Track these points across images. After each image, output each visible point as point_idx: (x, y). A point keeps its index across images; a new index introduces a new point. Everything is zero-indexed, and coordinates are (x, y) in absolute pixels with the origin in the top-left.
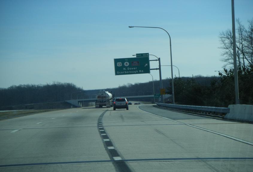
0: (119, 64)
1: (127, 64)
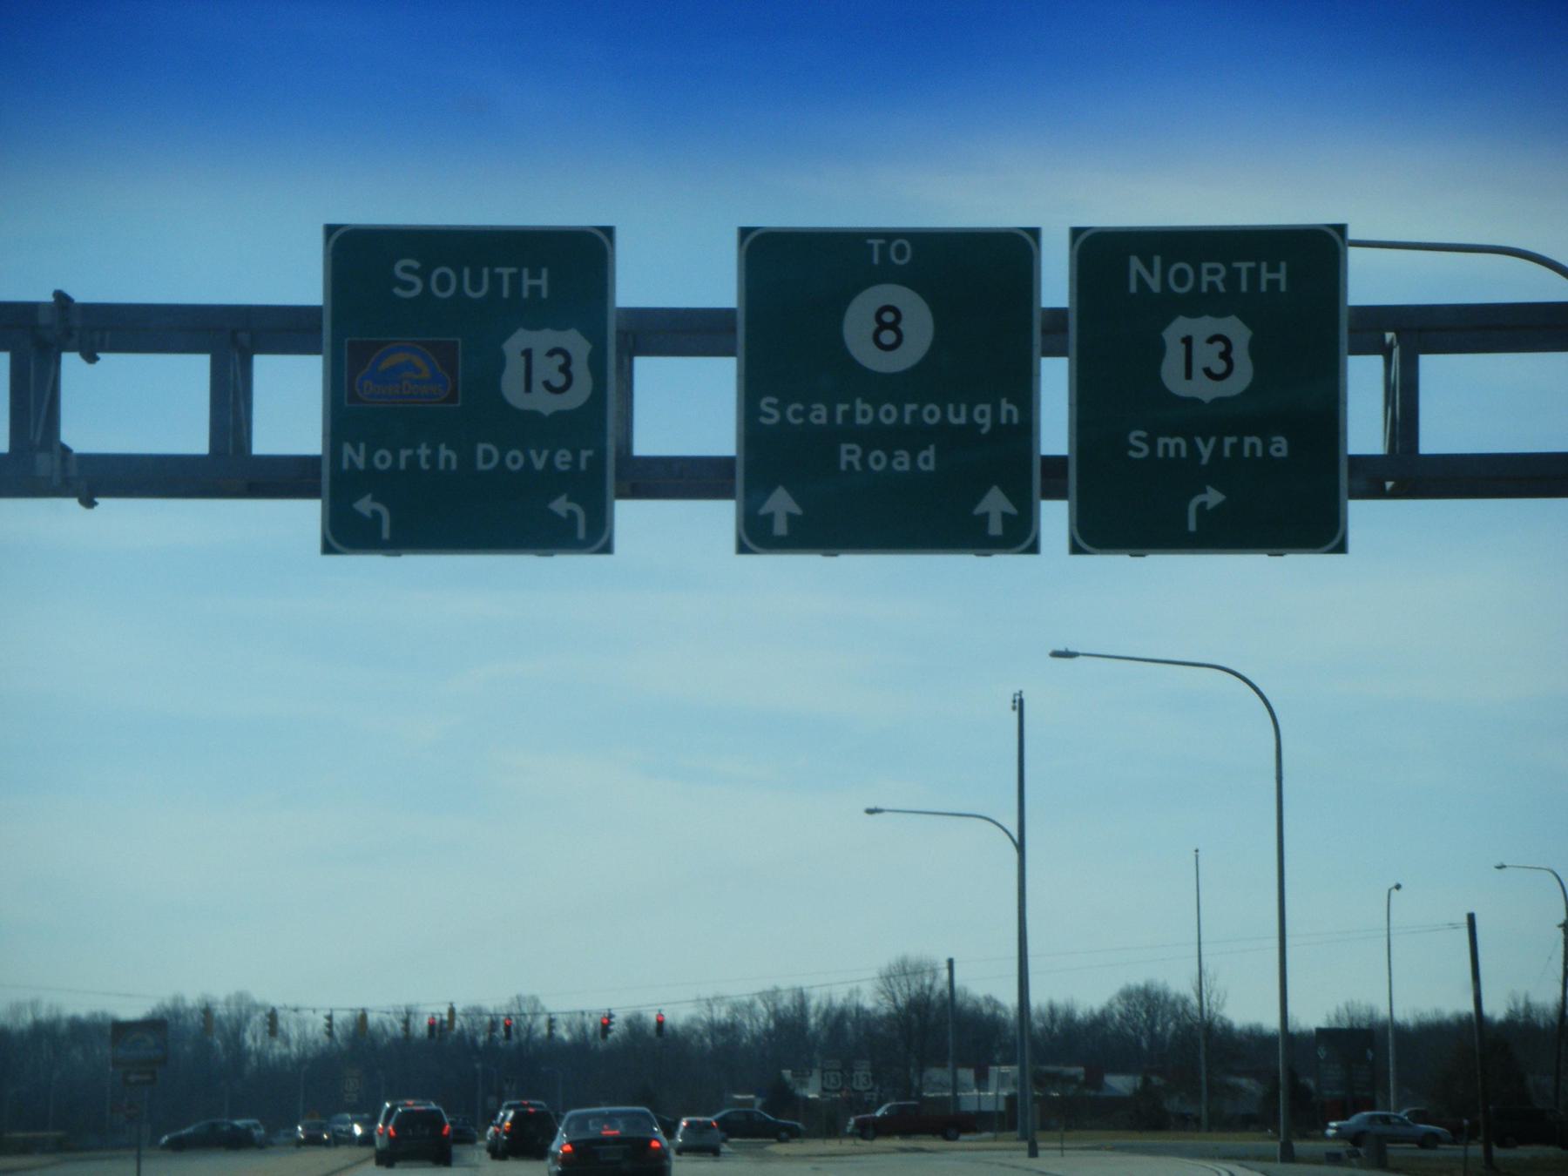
0: (547, 369)
1: (888, 322)
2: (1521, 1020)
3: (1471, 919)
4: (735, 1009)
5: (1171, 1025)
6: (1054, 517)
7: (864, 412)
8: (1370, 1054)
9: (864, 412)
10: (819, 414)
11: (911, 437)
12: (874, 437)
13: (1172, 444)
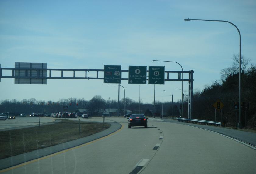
1: (138, 71)
2: (179, 103)
3: (172, 95)
4: (65, 100)
5: (130, 103)
6: (147, 81)
7: (136, 76)
8: (160, 108)
9: (136, 76)
10: (134, 76)
11: (139, 77)
12: (137, 77)
13: (154, 78)
